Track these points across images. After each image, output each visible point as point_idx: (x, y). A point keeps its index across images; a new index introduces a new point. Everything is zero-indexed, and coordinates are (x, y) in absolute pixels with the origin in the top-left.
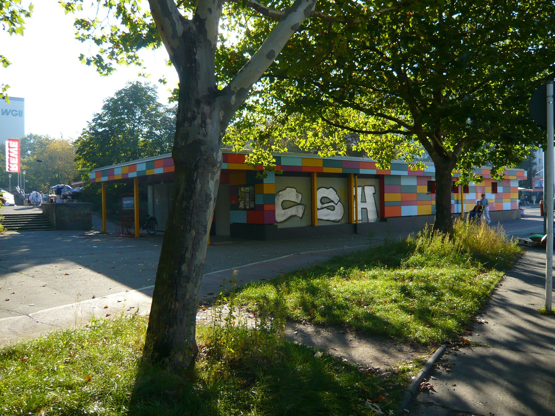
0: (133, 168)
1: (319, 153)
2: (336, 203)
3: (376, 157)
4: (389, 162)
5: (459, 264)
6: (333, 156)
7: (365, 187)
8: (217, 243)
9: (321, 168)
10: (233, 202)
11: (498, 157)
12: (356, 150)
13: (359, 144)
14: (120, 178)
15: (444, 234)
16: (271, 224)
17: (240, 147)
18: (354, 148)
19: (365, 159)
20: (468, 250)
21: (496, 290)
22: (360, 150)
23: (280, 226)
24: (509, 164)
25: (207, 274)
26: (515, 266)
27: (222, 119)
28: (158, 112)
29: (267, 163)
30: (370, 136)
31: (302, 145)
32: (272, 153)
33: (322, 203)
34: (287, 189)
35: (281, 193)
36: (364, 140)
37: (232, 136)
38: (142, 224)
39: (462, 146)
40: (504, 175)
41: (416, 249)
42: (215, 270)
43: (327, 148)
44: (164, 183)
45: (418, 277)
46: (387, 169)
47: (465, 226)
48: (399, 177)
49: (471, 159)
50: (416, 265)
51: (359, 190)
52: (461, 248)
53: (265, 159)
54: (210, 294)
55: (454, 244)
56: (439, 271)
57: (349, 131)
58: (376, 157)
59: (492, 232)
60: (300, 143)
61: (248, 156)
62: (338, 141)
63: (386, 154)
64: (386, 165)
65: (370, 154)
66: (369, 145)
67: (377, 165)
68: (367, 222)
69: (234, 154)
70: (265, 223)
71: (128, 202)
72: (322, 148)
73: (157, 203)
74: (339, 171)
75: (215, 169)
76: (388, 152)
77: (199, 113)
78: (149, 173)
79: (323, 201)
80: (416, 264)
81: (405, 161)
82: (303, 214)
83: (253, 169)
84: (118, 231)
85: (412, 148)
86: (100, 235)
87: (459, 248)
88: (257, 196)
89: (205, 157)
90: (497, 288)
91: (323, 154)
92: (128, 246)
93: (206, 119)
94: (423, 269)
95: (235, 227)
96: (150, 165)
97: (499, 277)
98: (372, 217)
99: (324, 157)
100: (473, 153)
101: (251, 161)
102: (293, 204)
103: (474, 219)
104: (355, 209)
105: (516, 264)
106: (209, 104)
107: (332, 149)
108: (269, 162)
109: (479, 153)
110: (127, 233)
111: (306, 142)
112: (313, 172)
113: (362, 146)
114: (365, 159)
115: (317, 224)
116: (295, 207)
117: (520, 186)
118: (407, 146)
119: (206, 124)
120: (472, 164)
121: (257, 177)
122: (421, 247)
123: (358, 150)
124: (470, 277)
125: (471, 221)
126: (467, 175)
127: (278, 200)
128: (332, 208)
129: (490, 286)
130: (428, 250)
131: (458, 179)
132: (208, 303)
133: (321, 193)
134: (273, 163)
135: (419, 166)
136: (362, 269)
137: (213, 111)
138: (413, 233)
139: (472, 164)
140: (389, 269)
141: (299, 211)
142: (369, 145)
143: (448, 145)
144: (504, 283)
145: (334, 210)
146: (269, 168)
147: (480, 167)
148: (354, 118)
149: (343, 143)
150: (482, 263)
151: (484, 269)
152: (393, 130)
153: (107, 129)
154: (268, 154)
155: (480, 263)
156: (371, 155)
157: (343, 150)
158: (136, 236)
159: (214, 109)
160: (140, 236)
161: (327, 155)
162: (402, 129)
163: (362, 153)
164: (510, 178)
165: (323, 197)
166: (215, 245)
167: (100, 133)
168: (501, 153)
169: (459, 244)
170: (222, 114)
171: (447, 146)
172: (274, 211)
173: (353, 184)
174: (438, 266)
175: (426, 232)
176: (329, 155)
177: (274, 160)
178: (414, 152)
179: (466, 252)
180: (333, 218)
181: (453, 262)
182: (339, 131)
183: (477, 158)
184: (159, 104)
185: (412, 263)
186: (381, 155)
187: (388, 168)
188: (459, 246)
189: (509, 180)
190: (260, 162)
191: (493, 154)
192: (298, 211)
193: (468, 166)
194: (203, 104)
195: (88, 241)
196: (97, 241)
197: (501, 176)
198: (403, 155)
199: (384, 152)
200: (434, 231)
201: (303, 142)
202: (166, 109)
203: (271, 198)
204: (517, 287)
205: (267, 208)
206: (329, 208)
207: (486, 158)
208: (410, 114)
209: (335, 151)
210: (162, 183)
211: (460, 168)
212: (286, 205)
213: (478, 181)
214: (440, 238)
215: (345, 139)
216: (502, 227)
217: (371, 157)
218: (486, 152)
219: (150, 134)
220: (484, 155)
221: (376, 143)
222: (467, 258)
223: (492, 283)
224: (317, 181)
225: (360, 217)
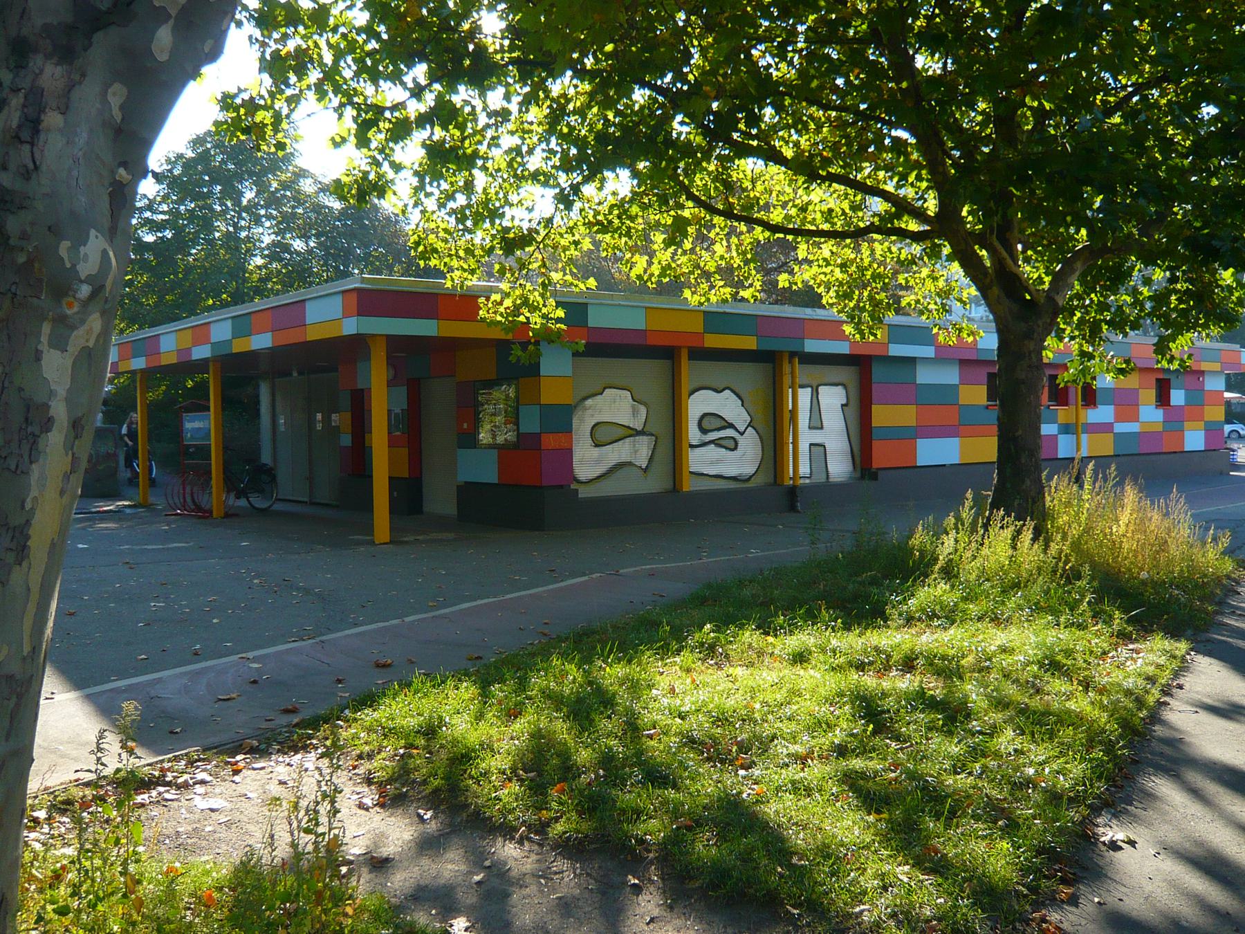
0: (200, 336)
1: (687, 293)
2: (742, 429)
3: (845, 306)
4: (881, 321)
5: (1056, 613)
6: (725, 301)
7: (821, 389)
8: (411, 538)
9: (700, 336)
10: (465, 426)
11: (1176, 307)
12: (787, 285)
13: (796, 268)
14: (173, 360)
15: (1019, 523)
16: (562, 487)
17: (466, 275)
18: (783, 280)
19: (819, 314)
20: (1086, 570)
21: (1166, 704)
22: (800, 285)
23: (584, 493)
24: (1205, 326)
25: (324, 638)
26: (1220, 618)
27: (119, 118)
28: (298, 192)
29: (539, 320)
30: (827, 248)
31: (638, 270)
32: (554, 294)
33: (704, 431)
34: (608, 391)
35: (589, 402)
36: (811, 257)
37: (443, 245)
38: (230, 483)
39: (1073, 271)
40: (1190, 356)
41: (937, 568)
42: (356, 625)
43: (708, 280)
44: (300, 373)
45: (930, 659)
46: (872, 338)
47: (1080, 499)
48: (911, 361)
49: (1102, 314)
50: (933, 616)
51: (804, 396)
52: (1066, 563)
53: (534, 308)
54: (287, 711)
55: (1045, 551)
56: (996, 638)
57: (767, 234)
58: (845, 306)
59: (1156, 516)
60: (633, 265)
61: (488, 299)
62: (738, 261)
63: (871, 298)
64: (870, 328)
65: (829, 298)
66: (825, 274)
67: (848, 329)
68: (823, 480)
69: (450, 296)
70: (544, 484)
71: (197, 425)
72: (693, 281)
73: (282, 429)
74: (750, 343)
75: (70, 305)
76: (878, 294)
77: (16, 90)
78: (239, 347)
79: (705, 425)
80: (933, 611)
81: (924, 317)
82: (651, 460)
83: (502, 336)
84: (171, 502)
85: (941, 283)
86: (128, 511)
87: (1061, 564)
88: (523, 410)
89: (21, 259)
90: (1167, 699)
91: (696, 298)
92: (150, 547)
93: (42, 111)
94: (952, 631)
95: (470, 494)
96: (243, 326)
97: (1175, 657)
98: (839, 467)
99: (701, 304)
100: (1106, 297)
101: (495, 313)
102: (621, 432)
103: (1105, 479)
104: (791, 446)
105: (1222, 614)
106: (66, 54)
107: (722, 283)
108: (545, 316)
109: (1124, 297)
110: (193, 507)
111: (650, 263)
112: (680, 348)
113: (805, 275)
114: (819, 314)
115: (688, 485)
116: (628, 440)
117: (1229, 389)
118: (929, 276)
119: (36, 131)
120: (1105, 327)
121: (512, 359)
122: (951, 560)
123: (794, 287)
124: (1087, 657)
125: (1097, 485)
126: (1091, 357)
127: (582, 420)
128: (731, 444)
129: (1147, 692)
130: (970, 570)
131: (1065, 368)
132: (263, 746)
133: (698, 405)
134: (558, 320)
135: (960, 330)
136: (766, 628)
137: (80, 83)
138: (931, 518)
139: (1105, 327)
140: (847, 627)
141: (639, 451)
142: (825, 274)
143: (1034, 271)
144: (1187, 680)
145: (735, 448)
146: (546, 336)
147: (1126, 335)
148: (781, 198)
149: (752, 265)
150: (1126, 611)
151: (1131, 629)
152: (885, 227)
153: (168, 234)
154: (542, 295)
155: (1117, 614)
156: (830, 301)
157: (751, 285)
158: (215, 514)
159: (83, 75)
160: (227, 515)
161: (708, 300)
162: (913, 226)
163: (809, 297)
164: (1204, 366)
165: (705, 415)
166: (407, 542)
167: (148, 246)
168: (1184, 296)
169: (1061, 551)
170: (117, 96)
171: (1036, 276)
172: (569, 452)
173: (787, 380)
174: (996, 620)
175: (966, 514)
176: (714, 299)
177: (560, 313)
178: (945, 294)
179: (1079, 578)
180: (732, 471)
181: (1038, 609)
182: (741, 233)
183: (1116, 311)
184: (301, 170)
185: (923, 610)
186: (859, 301)
187: (875, 335)
188: (1060, 559)
189: (1202, 373)
190: (522, 319)
191: (1160, 298)
192: (636, 452)
193: (1092, 332)
194: (41, 56)
195: (84, 528)
196: (106, 529)
197: (1182, 360)
198: (918, 302)
199: (866, 294)
200: (991, 514)
201: (641, 261)
202: (320, 182)
203: (561, 418)
204: (1229, 693)
205: (550, 441)
206: (723, 442)
207: (1142, 310)
208: (928, 180)
209: (728, 290)
210: (295, 374)
211: (1072, 338)
212: (603, 435)
213: (1121, 371)
214: (1008, 533)
215: (761, 253)
216: (1182, 500)
217: (831, 305)
218: (1141, 293)
219: (278, 251)
220: (1137, 303)
221: (843, 266)
222: (1083, 596)
223: (1151, 680)
224: (689, 371)
225: (804, 469)
